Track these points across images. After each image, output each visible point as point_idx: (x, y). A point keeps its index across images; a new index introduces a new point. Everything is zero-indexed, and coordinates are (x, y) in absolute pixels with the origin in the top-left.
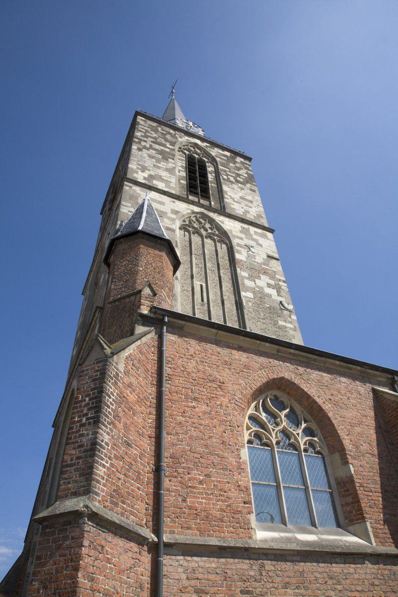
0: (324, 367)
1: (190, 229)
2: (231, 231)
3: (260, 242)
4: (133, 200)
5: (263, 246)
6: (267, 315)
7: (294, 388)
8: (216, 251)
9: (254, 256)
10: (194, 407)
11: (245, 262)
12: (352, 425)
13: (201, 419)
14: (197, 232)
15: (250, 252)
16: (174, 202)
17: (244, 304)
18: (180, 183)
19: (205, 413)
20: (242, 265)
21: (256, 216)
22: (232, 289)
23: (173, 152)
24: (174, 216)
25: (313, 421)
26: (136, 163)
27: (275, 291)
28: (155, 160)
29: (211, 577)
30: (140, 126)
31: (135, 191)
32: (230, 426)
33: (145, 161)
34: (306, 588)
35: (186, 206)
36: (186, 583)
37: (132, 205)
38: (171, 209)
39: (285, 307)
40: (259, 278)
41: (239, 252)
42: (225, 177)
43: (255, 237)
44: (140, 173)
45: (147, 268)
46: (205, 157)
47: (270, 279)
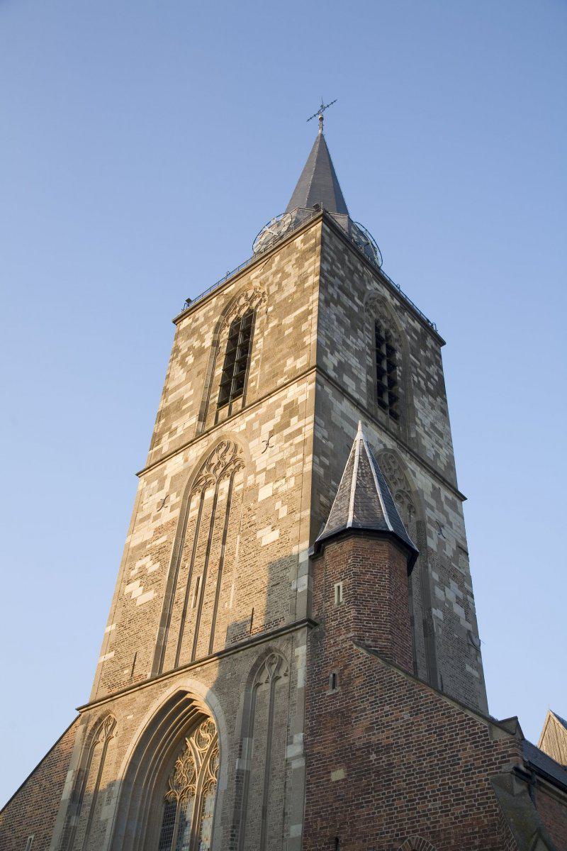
9: (445, 543)
15: (441, 537)
31: (327, 395)
35: (378, 436)
42: (416, 379)
43: (446, 508)
44: (329, 355)
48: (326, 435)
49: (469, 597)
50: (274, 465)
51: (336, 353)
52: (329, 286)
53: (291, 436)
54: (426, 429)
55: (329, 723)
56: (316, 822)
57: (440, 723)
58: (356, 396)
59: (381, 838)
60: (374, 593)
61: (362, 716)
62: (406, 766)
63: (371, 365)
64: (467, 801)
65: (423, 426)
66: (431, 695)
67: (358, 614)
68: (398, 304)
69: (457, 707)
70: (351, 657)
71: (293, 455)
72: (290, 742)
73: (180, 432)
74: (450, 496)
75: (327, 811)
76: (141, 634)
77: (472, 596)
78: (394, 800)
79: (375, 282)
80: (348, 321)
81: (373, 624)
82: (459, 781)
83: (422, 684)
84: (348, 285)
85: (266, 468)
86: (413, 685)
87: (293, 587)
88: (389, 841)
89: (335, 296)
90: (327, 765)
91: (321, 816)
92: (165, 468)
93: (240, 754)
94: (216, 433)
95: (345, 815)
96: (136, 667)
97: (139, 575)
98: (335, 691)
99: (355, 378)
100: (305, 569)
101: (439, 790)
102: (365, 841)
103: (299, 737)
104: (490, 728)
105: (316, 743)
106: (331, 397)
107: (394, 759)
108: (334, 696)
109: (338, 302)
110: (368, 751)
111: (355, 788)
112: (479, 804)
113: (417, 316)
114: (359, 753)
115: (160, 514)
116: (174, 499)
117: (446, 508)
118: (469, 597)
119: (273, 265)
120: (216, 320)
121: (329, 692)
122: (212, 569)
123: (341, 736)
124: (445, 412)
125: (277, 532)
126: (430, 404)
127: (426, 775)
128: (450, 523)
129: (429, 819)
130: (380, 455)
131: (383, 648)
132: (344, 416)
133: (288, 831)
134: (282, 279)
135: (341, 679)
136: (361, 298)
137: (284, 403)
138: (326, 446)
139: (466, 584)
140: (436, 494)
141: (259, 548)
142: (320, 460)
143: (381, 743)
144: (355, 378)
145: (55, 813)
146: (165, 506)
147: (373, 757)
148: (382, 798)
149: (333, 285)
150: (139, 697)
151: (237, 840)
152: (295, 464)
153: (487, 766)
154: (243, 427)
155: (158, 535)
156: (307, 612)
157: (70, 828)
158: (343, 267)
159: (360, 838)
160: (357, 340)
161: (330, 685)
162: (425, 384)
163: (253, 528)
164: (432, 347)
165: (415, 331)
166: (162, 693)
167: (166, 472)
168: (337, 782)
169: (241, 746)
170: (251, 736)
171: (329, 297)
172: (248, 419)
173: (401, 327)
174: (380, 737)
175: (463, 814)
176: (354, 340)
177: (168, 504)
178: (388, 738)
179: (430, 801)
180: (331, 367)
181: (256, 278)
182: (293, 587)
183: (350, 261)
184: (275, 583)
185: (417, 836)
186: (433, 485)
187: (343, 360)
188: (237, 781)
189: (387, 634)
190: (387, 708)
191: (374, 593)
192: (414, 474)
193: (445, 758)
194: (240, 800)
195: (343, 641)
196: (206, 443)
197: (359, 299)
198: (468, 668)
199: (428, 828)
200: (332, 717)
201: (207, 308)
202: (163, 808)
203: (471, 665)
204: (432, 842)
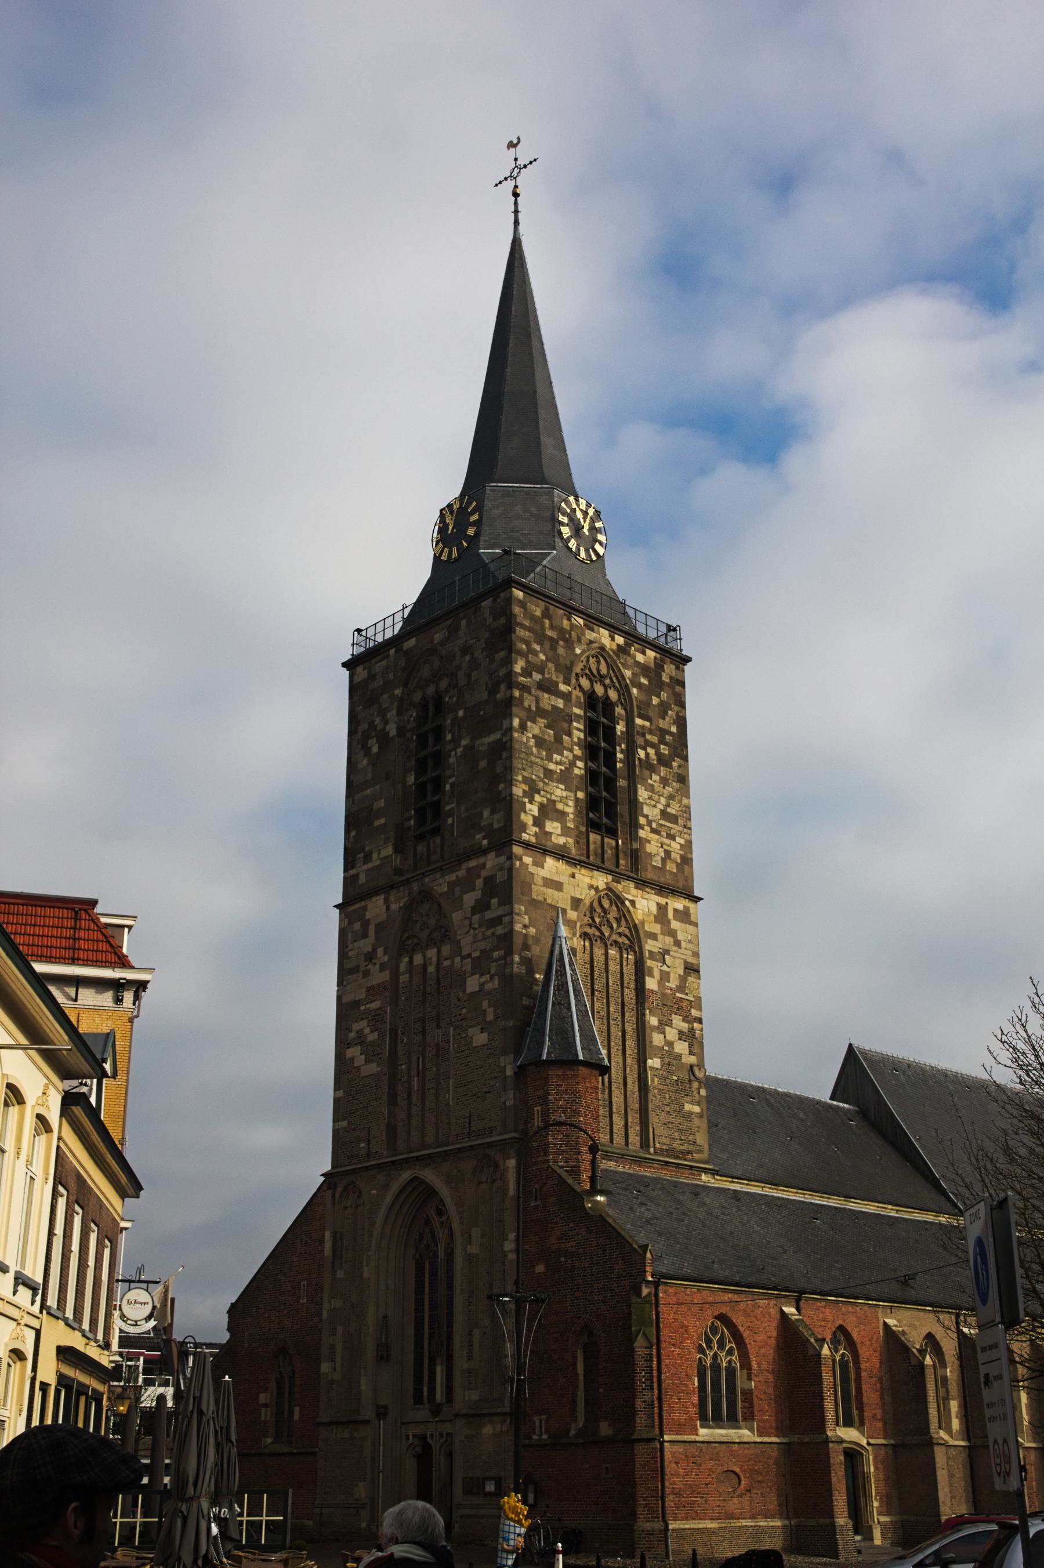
5: (683, 944)
6: (673, 1095)
8: (622, 973)
10: (673, 1351)
12: (760, 1347)
17: (650, 1084)
22: (636, 1051)
29: (681, 1456)
34: (719, 1460)
35: (587, 880)
36: (671, 1459)
37: (525, 907)
38: (572, 898)
40: (670, 1024)
93: (470, 1241)
103: (512, 1236)
121: (533, 1204)
124: (683, 779)
147: (563, 1259)
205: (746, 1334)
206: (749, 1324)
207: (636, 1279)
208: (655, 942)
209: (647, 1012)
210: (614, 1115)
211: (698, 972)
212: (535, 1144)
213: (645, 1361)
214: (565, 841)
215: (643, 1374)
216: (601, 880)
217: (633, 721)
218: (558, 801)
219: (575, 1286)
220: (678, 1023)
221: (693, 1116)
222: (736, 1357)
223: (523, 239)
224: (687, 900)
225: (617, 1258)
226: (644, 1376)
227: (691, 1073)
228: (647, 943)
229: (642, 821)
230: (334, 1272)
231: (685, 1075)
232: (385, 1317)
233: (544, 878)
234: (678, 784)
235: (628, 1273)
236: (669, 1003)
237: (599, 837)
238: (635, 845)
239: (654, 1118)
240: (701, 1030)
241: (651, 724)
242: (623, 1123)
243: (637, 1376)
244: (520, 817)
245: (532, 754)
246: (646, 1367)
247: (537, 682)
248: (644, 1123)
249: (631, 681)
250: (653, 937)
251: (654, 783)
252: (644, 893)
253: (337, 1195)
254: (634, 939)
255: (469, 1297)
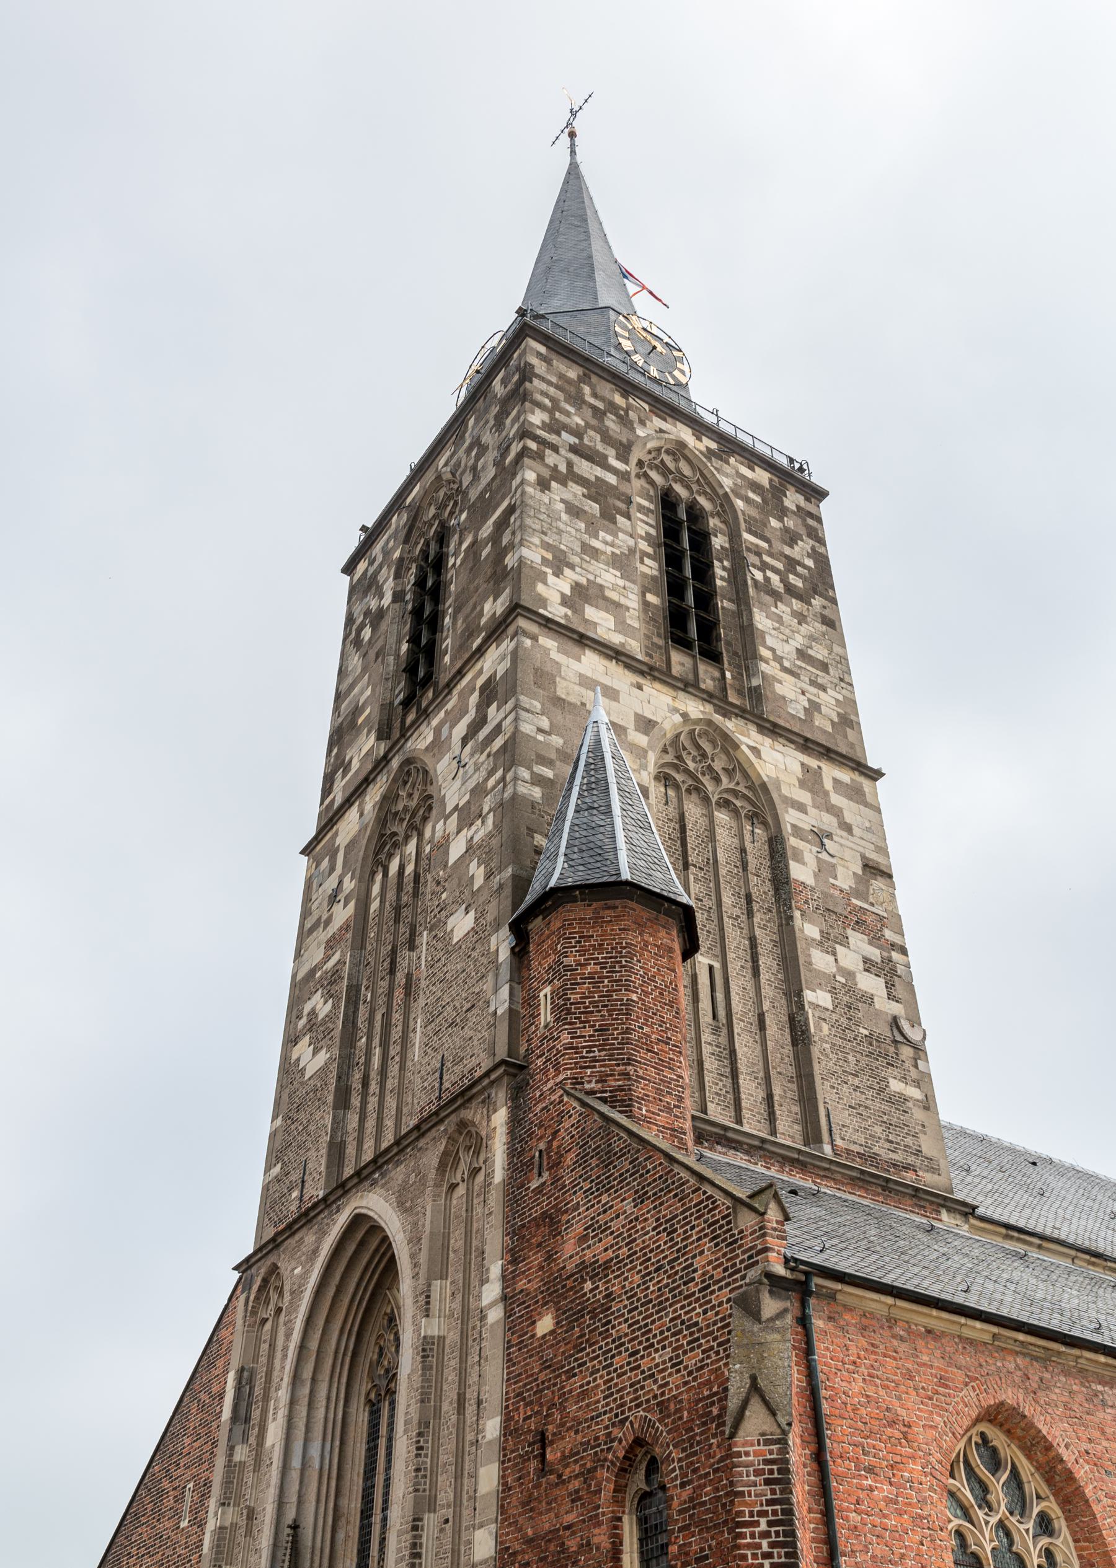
0: (1074, 1367)
1: (679, 777)
2: (778, 783)
3: (848, 817)
4: (544, 689)
5: (856, 831)
6: (864, 1061)
7: (1023, 1425)
9: (834, 866)
10: (871, 1489)
11: (813, 889)
13: (885, 1516)
14: (697, 789)
15: (824, 856)
16: (640, 687)
17: (812, 1030)
18: (646, 604)
19: (889, 1501)
20: (806, 902)
21: (836, 720)
23: (624, 488)
24: (642, 740)
25: (1052, 1498)
26: (536, 541)
27: (881, 981)
28: (582, 526)
30: (536, 382)
31: (547, 651)
32: (929, 1528)
33: (560, 532)
35: (669, 700)
37: (543, 705)
38: (636, 714)
39: (905, 1038)
40: (844, 941)
41: (800, 860)
42: (759, 576)
43: (836, 799)
44: (551, 579)
45: (647, 994)
46: (705, 493)
47: (870, 943)
48: (545, 723)
49: (896, 956)
50: (467, 797)
51: (567, 571)
52: (548, 452)
53: (490, 739)
54: (786, 664)
55: (534, 1236)
56: (518, 1409)
57: (671, 1212)
58: (616, 639)
59: (597, 1424)
60: (601, 996)
61: (574, 1218)
62: (629, 1294)
63: (655, 573)
64: (703, 1341)
65: (778, 659)
66: (661, 1164)
67: (572, 1038)
68: (713, 446)
69: (692, 1181)
70: (561, 1115)
71: (491, 773)
72: (483, 1281)
73: (355, 765)
74: (845, 776)
75: (532, 1388)
76: (312, 1128)
77: (904, 951)
78: (613, 1357)
79: (655, 419)
80: (594, 508)
81: (599, 1051)
82: (694, 1309)
83: (649, 1147)
84: (593, 439)
85: (458, 805)
86: (638, 1151)
87: (492, 1009)
88: (607, 1427)
89: (563, 468)
90: (532, 1311)
91: (524, 1399)
92: (336, 834)
93: (427, 1310)
94: (397, 757)
95: (553, 1392)
96: (307, 1185)
97: (308, 1027)
98: (542, 1180)
99: (615, 607)
100: (505, 973)
101: (669, 1329)
102: (577, 1432)
103: (495, 1270)
104: (734, 1208)
105: (518, 1275)
106: (555, 655)
107: (613, 1285)
108: (539, 1190)
109: (571, 476)
110: (582, 1277)
111: (566, 1344)
112: (719, 1345)
113: (753, 458)
114: (569, 1283)
115: (331, 915)
116: (349, 885)
117: (836, 799)
118: (896, 956)
119: (467, 435)
120: (397, 554)
121: (534, 1185)
122: (399, 995)
123: (549, 1257)
124: (831, 623)
125: (472, 914)
126: (796, 614)
127: (654, 1307)
128: (848, 828)
129: (655, 1382)
130: (678, 736)
131: (616, 1090)
132: (587, 682)
133: (483, 1431)
134: (478, 458)
135: (549, 1158)
136: (623, 457)
137: (480, 682)
138: (547, 745)
139: (888, 934)
140: (810, 780)
141: (450, 949)
142: (532, 773)
143: (597, 1261)
144: (615, 607)
145: (215, 1444)
146: (338, 899)
147: (588, 1285)
148: (598, 1356)
149: (555, 449)
150: (309, 1237)
151: (426, 1456)
152: (494, 787)
153: (730, 1276)
154: (430, 738)
155: (330, 952)
156: (509, 1044)
157: (235, 1466)
158: (579, 409)
159: (570, 1428)
160: (616, 536)
161: (536, 1171)
162: (782, 581)
163: (444, 913)
164: (798, 507)
165: (755, 486)
166: (334, 1221)
167: (338, 841)
168: (544, 1336)
169: (428, 1297)
170: (974, 1208)
171: (546, 473)
172: (435, 722)
173: (722, 487)
174: (598, 1251)
175: (699, 1365)
176: (609, 538)
177: (341, 897)
178: (606, 1250)
179: (657, 1351)
180: (554, 598)
181: (446, 464)
182: (492, 1009)
183: (595, 395)
184: (469, 1005)
185: (641, 1413)
186: (803, 764)
187: (584, 581)
188: (423, 1357)
189: (624, 1064)
190: (605, 1198)
191: (601, 996)
192: (755, 751)
193: (676, 1273)
194: (430, 1381)
195: (552, 1091)
196: (385, 779)
197: (617, 459)
198: (896, 1086)
199: (655, 1397)
200: (538, 1226)
201: (385, 537)
202: (366, 1414)
203: (904, 1079)
204: (660, 1421)
205: (1082, 1472)
206: (1085, 1446)
207: (743, 1277)
208: (804, 815)
209: (797, 914)
210: (741, 1077)
211: (890, 876)
212: (539, 1062)
213: (767, 1482)
214: (623, 641)
215: (763, 1526)
216: (695, 709)
217: (740, 536)
218: (608, 588)
219: (614, 1341)
220: (859, 943)
221: (910, 1104)
222: (1065, 1541)
223: (582, 168)
224: (856, 773)
225: (699, 1239)
226: (765, 1535)
227: (894, 1025)
228: (787, 812)
229: (764, 652)
230: (231, 1449)
231: (884, 1030)
232: (295, 1527)
233: (581, 675)
234: (824, 627)
235: (725, 1270)
236: (839, 910)
237: (688, 661)
238: (755, 682)
239: (824, 1092)
240: (908, 966)
241: (769, 546)
242: (761, 1094)
243: (742, 1536)
244: (535, 587)
245: (560, 519)
246: (770, 1502)
247: (570, 444)
248: (807, 1098)
249: (732, 491)
250: (801, 808)
251: (781, 614)
252: (776, 743)
253: (252, 1298)
254: (763, 805)
255: (420, 1434)
